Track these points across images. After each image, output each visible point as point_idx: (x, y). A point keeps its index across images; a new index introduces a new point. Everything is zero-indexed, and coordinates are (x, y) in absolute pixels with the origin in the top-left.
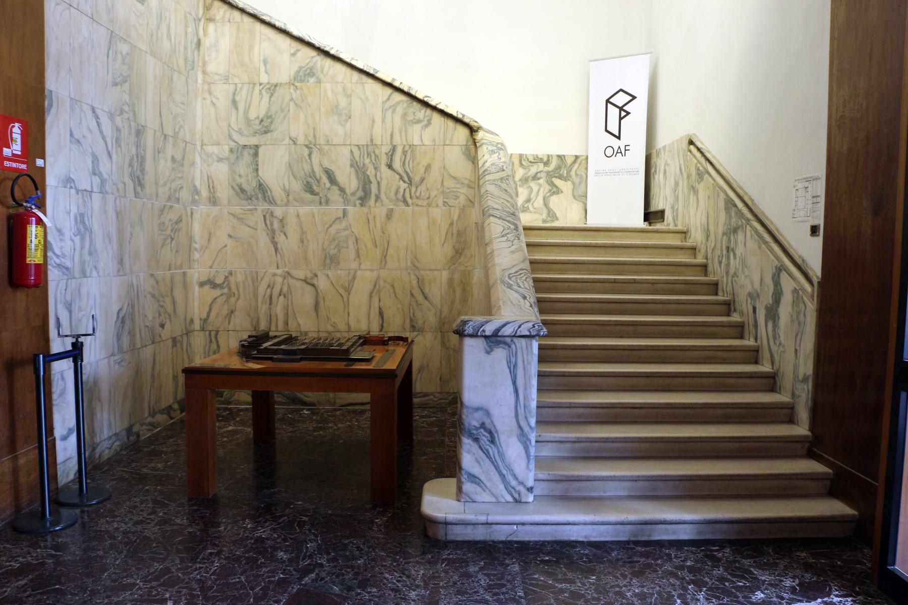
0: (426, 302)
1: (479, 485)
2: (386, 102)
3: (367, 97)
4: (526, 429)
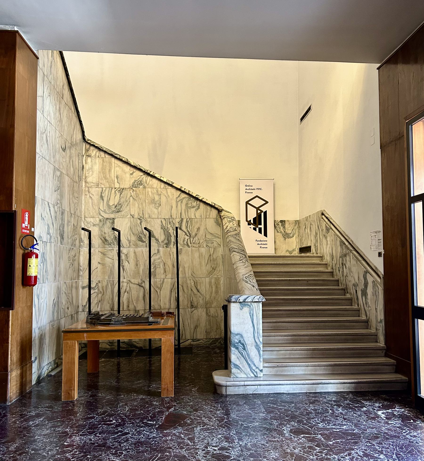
0: (199, 293)
1: (239, 369)
2: (178, 197)
3: (168, 196)
4: (258, 343)
